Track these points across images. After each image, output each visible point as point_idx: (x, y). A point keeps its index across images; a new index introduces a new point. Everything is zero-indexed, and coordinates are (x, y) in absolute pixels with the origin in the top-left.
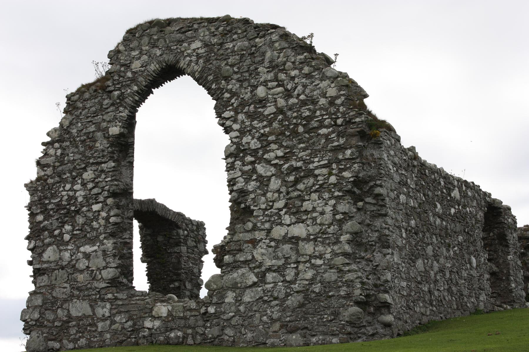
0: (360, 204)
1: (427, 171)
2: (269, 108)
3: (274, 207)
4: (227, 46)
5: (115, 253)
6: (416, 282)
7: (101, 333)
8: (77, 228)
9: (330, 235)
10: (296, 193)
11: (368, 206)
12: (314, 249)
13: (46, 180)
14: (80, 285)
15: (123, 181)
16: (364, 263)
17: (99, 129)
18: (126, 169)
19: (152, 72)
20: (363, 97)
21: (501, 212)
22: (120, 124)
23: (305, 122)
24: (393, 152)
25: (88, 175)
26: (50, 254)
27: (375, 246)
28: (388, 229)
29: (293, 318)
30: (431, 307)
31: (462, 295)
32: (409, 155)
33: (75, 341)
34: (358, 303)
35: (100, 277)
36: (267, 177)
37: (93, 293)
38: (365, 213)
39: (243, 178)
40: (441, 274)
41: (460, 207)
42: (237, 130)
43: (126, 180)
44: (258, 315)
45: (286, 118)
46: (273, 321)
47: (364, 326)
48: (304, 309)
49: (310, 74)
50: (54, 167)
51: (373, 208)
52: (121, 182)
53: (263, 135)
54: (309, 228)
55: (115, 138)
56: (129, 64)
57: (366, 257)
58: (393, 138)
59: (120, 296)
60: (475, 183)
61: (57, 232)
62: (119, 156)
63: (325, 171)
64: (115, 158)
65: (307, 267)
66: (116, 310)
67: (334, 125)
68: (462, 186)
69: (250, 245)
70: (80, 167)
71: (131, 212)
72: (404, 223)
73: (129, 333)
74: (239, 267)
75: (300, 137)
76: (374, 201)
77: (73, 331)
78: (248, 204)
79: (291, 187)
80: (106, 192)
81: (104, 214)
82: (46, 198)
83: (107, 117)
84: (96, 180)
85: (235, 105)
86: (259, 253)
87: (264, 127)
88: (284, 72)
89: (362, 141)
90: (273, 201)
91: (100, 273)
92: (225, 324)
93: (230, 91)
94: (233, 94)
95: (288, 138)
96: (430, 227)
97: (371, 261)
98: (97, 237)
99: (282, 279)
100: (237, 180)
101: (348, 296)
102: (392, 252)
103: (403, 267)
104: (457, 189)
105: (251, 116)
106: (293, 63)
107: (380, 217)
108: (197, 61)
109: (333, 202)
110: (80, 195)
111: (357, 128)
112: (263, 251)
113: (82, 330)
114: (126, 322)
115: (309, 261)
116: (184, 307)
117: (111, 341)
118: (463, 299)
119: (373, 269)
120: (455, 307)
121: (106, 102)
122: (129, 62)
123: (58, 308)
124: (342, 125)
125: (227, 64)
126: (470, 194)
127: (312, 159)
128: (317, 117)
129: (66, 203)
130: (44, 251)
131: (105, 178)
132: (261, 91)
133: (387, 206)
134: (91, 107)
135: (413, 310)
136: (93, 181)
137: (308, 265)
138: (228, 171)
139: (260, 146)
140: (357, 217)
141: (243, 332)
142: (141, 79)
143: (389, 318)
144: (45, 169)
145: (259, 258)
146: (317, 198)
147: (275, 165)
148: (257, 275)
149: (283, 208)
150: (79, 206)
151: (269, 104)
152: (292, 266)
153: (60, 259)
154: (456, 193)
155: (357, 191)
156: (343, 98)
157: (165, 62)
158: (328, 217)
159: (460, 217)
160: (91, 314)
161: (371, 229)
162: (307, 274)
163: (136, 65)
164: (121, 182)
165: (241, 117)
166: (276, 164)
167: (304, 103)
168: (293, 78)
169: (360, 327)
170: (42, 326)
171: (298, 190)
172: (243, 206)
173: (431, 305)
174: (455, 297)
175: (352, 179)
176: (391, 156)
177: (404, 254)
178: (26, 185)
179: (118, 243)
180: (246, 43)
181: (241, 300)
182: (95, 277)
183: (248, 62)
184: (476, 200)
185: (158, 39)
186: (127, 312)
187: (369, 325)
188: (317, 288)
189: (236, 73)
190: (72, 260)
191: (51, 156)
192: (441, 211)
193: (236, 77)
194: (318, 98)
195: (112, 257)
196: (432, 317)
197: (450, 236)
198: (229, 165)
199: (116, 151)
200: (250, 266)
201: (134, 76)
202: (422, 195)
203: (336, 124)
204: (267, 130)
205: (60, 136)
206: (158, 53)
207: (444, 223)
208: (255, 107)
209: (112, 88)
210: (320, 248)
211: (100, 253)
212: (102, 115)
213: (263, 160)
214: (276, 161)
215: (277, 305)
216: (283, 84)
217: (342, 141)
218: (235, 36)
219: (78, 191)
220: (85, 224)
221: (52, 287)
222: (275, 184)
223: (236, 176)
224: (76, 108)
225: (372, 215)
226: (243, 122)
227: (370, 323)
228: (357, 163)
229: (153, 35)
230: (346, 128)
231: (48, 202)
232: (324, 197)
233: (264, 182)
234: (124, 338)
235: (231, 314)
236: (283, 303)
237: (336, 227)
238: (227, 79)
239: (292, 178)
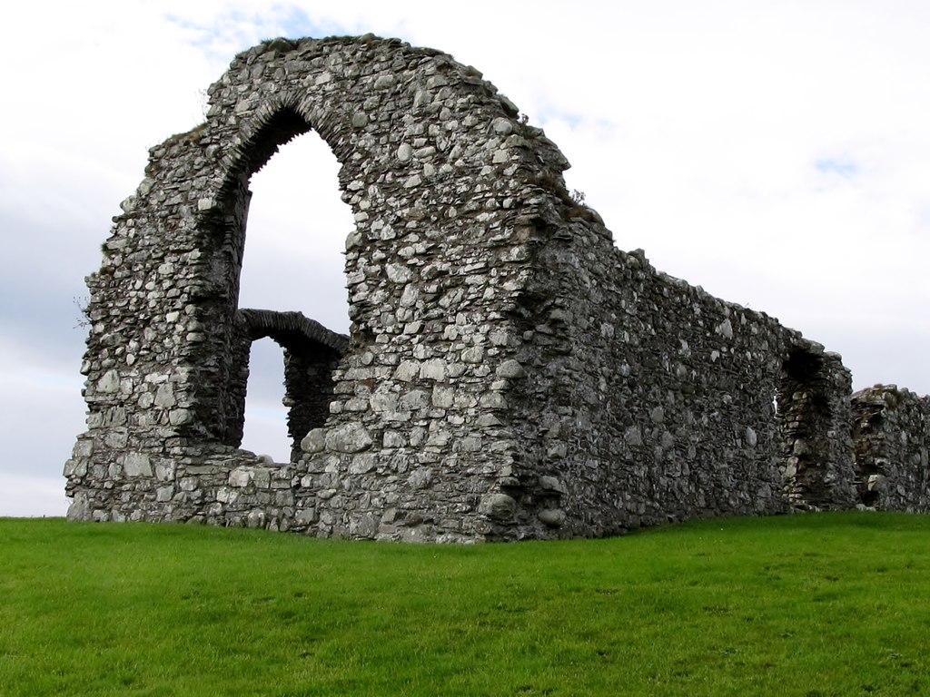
0: (528, 333)
1: (665, 290)
2: (412, 178)
3: (405, 332)
4: (365, 81)
6: (622, 461)
7: (160, 505)
8: (144, 347)
9: (478, 380)
10: (435, 312)
12: (453, 399)
13: (112, 273)
14: (141, 431)
16: (525, 426)
17: (186, 201)
19: (262, 118)
20: (560, 167)
21: (821, 363)
22: (214, 194)
23: (459, 202)
24: (594, 256)
25: (165, 268)
26: (106, 383)
27: (546, 400)
28: (570, 375)
29: (413, 504)
30: (649, 503)
31: (720, 486)
32: (628, 261)
33: (128, 512)
34: (505, 488)
35: (167, 420)
36: (399, 284)
37: (156, 443)
39: (368, 285)
40: (679, 452)
41: (732, 350)
42: (365, 210)
44: (367, 495)
45: (435, 195)
46: (387, 505)
47: (515, 525)
48: (431, 492)
49: (472, 127)
50: (124, 255)
51: (548, 341)
52: (209, 281)
53: (399, 219)
54: (449, 366)
56: (234, 104)
57: (530, 418)
58: (596, 233)
59: (191, 451)
60: (767, 313)
61: (118, 351)
62: (211, 242)
63: (480, 279)
65: (441, 428)
66: (183, 472)
67: (498, 209)
68: (740, 318)
69: (367, 387)
70: (157, 256)
72: (604, 369)
73: (196, 507)
74: (348, 420)
75: (450, 225)
76: (549, 331)
77: (126, 497)
78: (369, 324)
79: (431, 301)
80: (186, 296)
81: (180, 328)
82: (110, 300)
83: (197, 183)
84: (175, 277)
85: (366, 172)
86: (380, 401)
87: (403, 207)
88: (438, 122)
89: (539, 236)
90: (405, 322)
91: (168, 416)
92: (322, 505)
93: (361, 150)
94: (367, 155)
95: (434, 226)
96: (662, 377)
97: (537, 424)
98: (168, 361)
99: (405, 442)
100: (359, 286)
101: (492, 477)
102: (573, 412)
103: (594, 437)
104: (728, 321)
105: (387, 189)
106: (452, 109)
108: (323, 102)
109: (486, 327)
110: (153, 297)
112: (383, 397)
113: (137, 497)
114: (194, 490)
115: (444, 418)
116: (271, 475)
117: (172, 516)
118: (722, 493)
119: (538, 436)
120: (703, 503)
121: (197, 161)
122: (232, 102)
123: (111, 462)
124: (510, 209)
125: (361, 108)
126: (755, 330)
127: (464, 260)
128: (476, 194)
129: (134, 309)
130: (100, 377)
131: (186, 275)
132: (403, 152)
133: (572, 339)
134: (178, 167)
135: (611, 504)
136: (171, 278)
137: (443, 423)
138: (348, 272)
139: (393, 236)
141: (345, 520)
142: (246, 127)
143: (553, 514)
144: (113, 256)
145: (376, 407)
146: (465, 322)
147: (413, 267)
148: (371, 434)
149: (417, 333)
150: (149, 314)
151: (412, 172)
152: (421, 423)
153: (120, 389)
154: (725, 328)
156: (515, 166)
157: (281, 103)
158: (477, 351)
159: (732, 367)
160: (151, 475)
161: (543, 374)
162: (438, 438)
163: (242, 107)
165: (372, 189)
166: (414, 265)
167: (460, 172)
168: (449, 133)
169: (509, 526)
170: (88, 486)
171: (442, 307)
172: (362, 326)
173: (651, 498)
174: (703, 489)
175: (516, 294)
176: (588, 261)
177: (599, 416)
178: (87, 280)
180: (390, 77)
181: (346, 470)
182: (160, 420)
183: (390, 106)
184: (769, 342)
185: (275, 68)
186: (196, 475)
188: (451, 460)
189: (373, 122)
190: (133, 393)
191: (123, 238)
192: (690, 353)
193: (371, 127)
194: (480, 165)
196: (650, 517)
197: (705, 394)
198: (350, 264)
200: (364, 420)
201: (238, 123)
202: (649, 326)
203: (501, 208)
204: (406, 211)
205: (136, 208)
206: (273, 88)
207: (694, 373)
208: (394, 176)
209: (207, 140)
210: (462, 399)
211: (170, 387)
212: (192, 179)
214: (415, 260)
215: (394, 482)
216: (435, 142)
217: (507, 234)
218: (376, 67)
219: (151, 291)
220: (154, 341)
221: (106, 430)
222: (409, 295)
223: (358, 281)
224: (160, 169)
226: (375, 198)
227: (525, 522)
228: (526, 269)
229: (268, 62)
230: (516, 214)
231: (111, 305)
232: (475, 320)
233: (394, 290)
234: (189, 515)
235: (332, 491)
237: (486, 367)
238: (359, 131)
239: (433, 288)
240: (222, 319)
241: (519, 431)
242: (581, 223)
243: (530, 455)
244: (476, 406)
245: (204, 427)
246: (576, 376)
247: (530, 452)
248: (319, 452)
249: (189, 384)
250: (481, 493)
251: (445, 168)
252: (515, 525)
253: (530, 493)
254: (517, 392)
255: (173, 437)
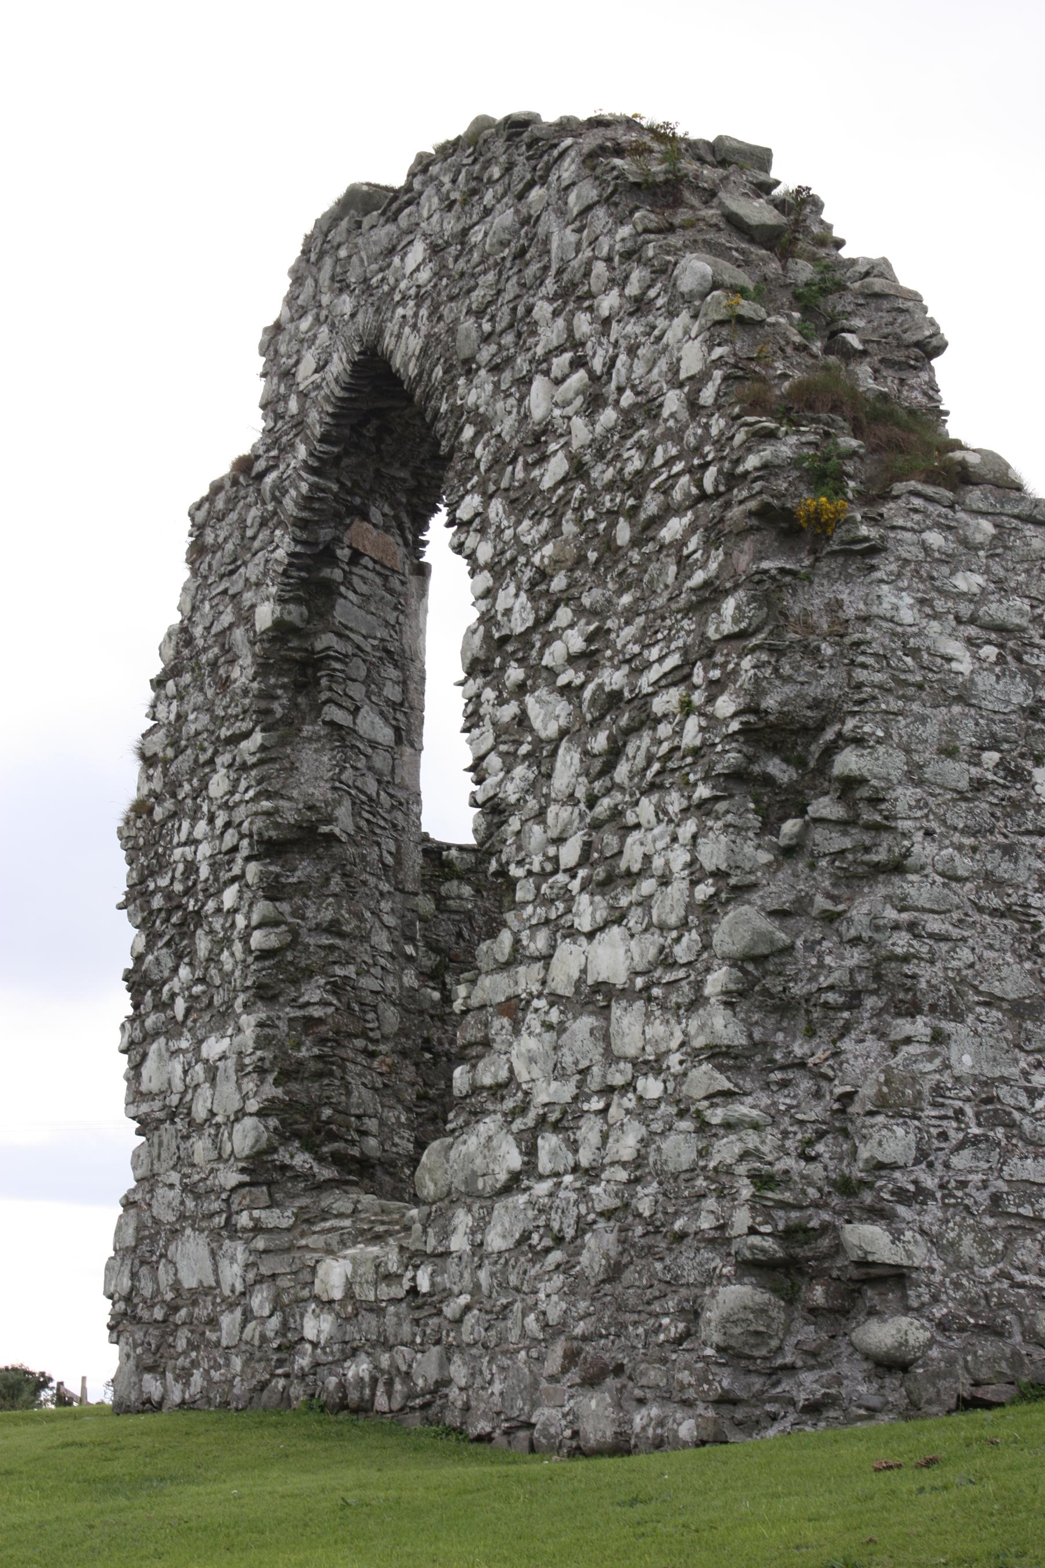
5: (262, 1059)
9: (681, 973)
11: (818, 834)
15: (295, 793)
16: (806, 1084)
18: (316, 751)
28: (912, 927)
38: (812, 867)
43: (311, 790)
47: (790, 1369)
51: (839, 842)
52: (290, 799)
54: (633, 943)
55: (269, 641)
64: (278, 716)
71: (329, 905)
89: (791, 552)
107: (881, 878)
111: (752, 497)
119: (835, 1112)
140: (773, 888)
149: (579, 865)
155: (776, 768)
160: (214, 1284)
164: (290, 799)
179: (280, 1024)
187: (811, 1362)
195: (255, 1075)
199: (283, 686)
213: (544, 675)
225: (841, 874)
227: (814, 1357)
236: (573, 1260)
240: (336, 883)
241: (783, 1101)
242: (917, 494)
243: (815, 1170)
244: (682, 1044)
245: (307, 1156)
246: (934, 924)
247: (809, 1159)
248: (441, 1200)
249: (259, 1053)
250: (704, 1285)
251: (608, 416)
252: (790, 1369)
253: (819, 1275)
254: (766, 992)
255: (241, 1185)
